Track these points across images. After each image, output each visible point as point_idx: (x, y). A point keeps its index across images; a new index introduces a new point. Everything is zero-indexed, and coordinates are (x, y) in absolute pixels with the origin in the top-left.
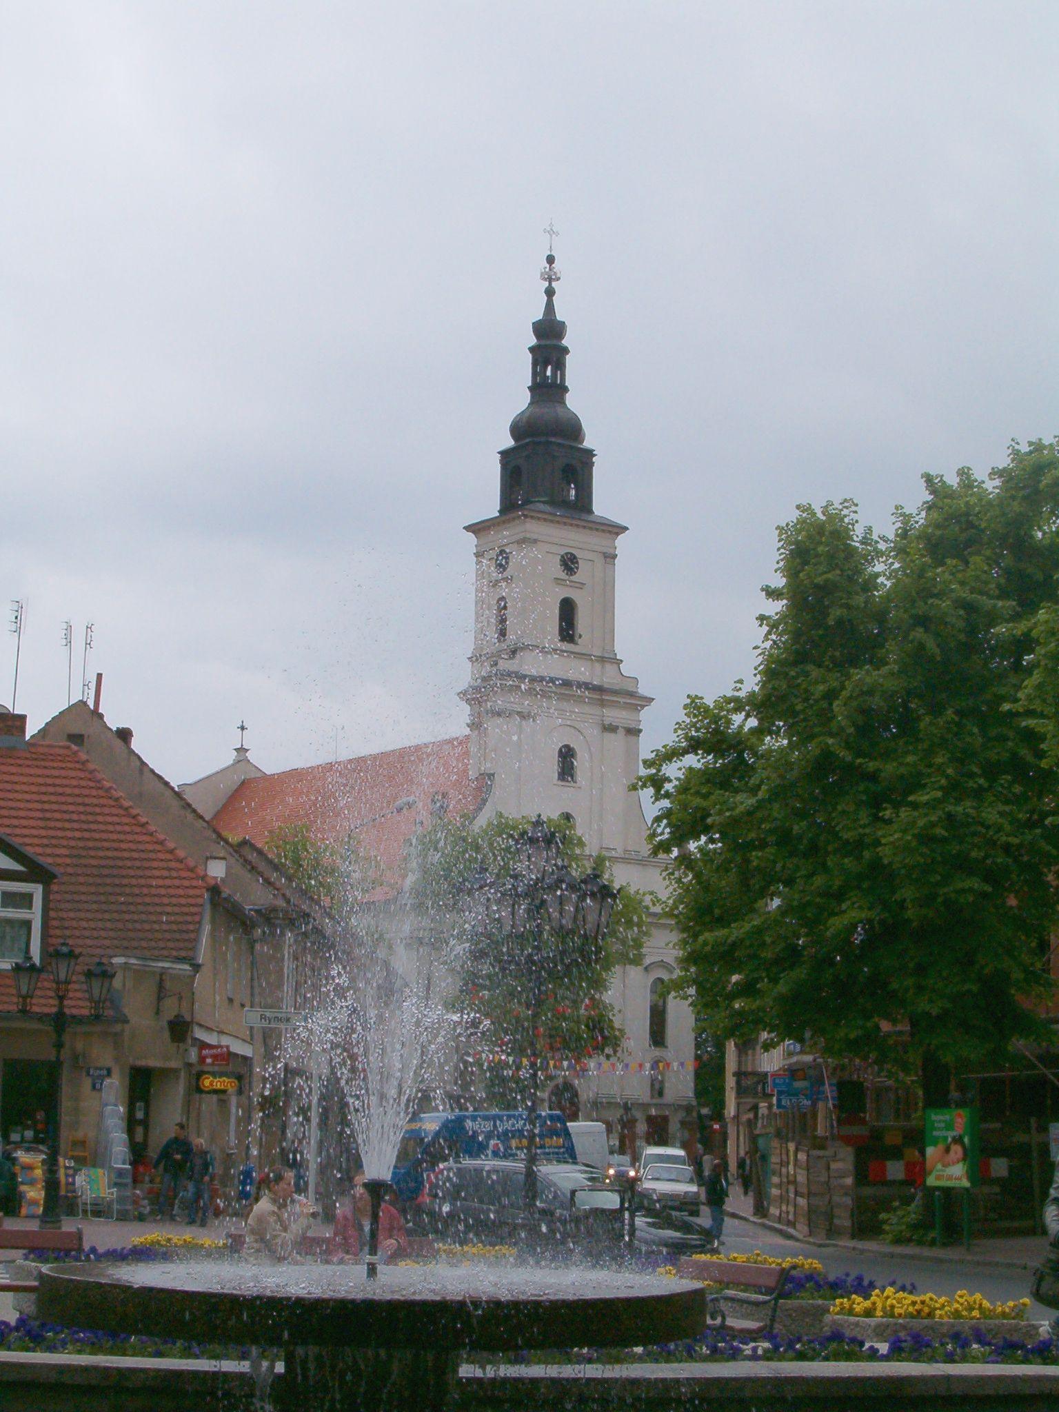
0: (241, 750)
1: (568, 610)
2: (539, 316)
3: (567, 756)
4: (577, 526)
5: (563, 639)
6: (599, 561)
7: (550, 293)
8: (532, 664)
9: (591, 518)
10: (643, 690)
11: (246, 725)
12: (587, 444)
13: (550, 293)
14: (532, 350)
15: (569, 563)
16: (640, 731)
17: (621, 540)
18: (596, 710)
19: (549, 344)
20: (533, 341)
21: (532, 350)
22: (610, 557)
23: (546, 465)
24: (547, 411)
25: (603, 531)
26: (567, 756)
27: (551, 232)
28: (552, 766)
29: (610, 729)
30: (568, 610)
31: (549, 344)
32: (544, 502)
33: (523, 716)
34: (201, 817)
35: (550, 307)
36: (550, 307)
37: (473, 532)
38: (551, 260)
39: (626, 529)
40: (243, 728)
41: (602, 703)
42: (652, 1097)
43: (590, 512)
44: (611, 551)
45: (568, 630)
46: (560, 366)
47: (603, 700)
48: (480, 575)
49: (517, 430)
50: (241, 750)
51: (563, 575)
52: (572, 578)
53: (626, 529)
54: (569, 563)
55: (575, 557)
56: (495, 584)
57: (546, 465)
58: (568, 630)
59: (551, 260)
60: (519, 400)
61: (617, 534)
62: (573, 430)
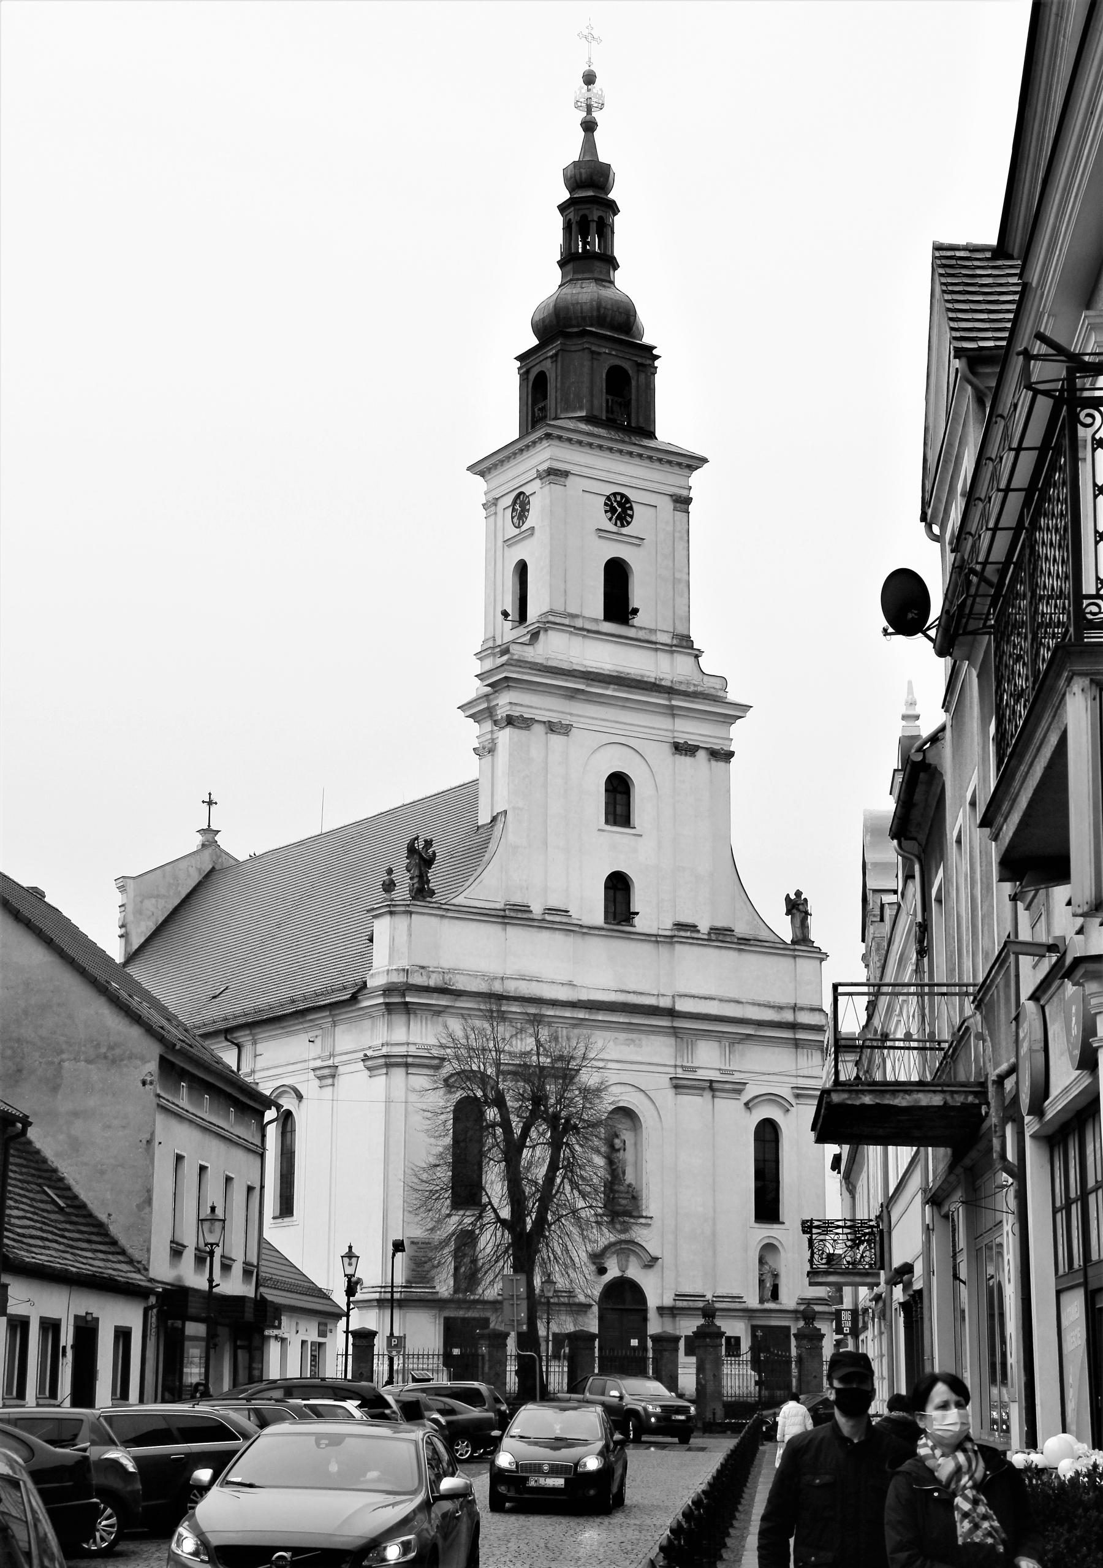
0: (209, 832)
1: (617, 575)
2: (574, 154)
3: (618, 787)
4: (631, 454)
5: (609, 616)
6: (666, 504)
7: (589, 126)
8: (557, 648)
9: (652, 444)
10: (734, 694)
11: (214, 798)
12: (647, 340)
13: (589, 126)
14: (562, 208)
15: (620, 509)
16: (731, 754)
17: (697, 479)
18: (663, 722)
19: (589, 204)
20: (565, 195)
21: (562, 208)
22: (683, 502)
23: (590, 370)
24: (587, 292)
25: (670, 462)
26: (618, 787)
27: (590, 38)
28: (595, 800)
29: (683, 749)
30: (617, 575)
31: (589, 204)
32: (580, 419)
33: (552, 727)
34: (406, 1110)
35: (589, 145)
36: (589, 145)
37: (482, 474)
38: (589, 79)
39: (705, 460)
40: (210, 803)
41: (672, 712)
42: (762, 1301)
43: (652, 435)
44: (684, 493)
45: (618, 604)
46: (605, 230)
47: (672, 707)
48: (492, 534)
50: (209, 832)
51: (610, 526)
52: (624, 530)
53: (705, 460)
54: (620, 509)
55: (628, 500)
56: (509, 542)
57: (590, 370)
58: (618, 604)
59: (589, 79)
60: (542, 281)
61: (692, 468)
62: (619, 324)
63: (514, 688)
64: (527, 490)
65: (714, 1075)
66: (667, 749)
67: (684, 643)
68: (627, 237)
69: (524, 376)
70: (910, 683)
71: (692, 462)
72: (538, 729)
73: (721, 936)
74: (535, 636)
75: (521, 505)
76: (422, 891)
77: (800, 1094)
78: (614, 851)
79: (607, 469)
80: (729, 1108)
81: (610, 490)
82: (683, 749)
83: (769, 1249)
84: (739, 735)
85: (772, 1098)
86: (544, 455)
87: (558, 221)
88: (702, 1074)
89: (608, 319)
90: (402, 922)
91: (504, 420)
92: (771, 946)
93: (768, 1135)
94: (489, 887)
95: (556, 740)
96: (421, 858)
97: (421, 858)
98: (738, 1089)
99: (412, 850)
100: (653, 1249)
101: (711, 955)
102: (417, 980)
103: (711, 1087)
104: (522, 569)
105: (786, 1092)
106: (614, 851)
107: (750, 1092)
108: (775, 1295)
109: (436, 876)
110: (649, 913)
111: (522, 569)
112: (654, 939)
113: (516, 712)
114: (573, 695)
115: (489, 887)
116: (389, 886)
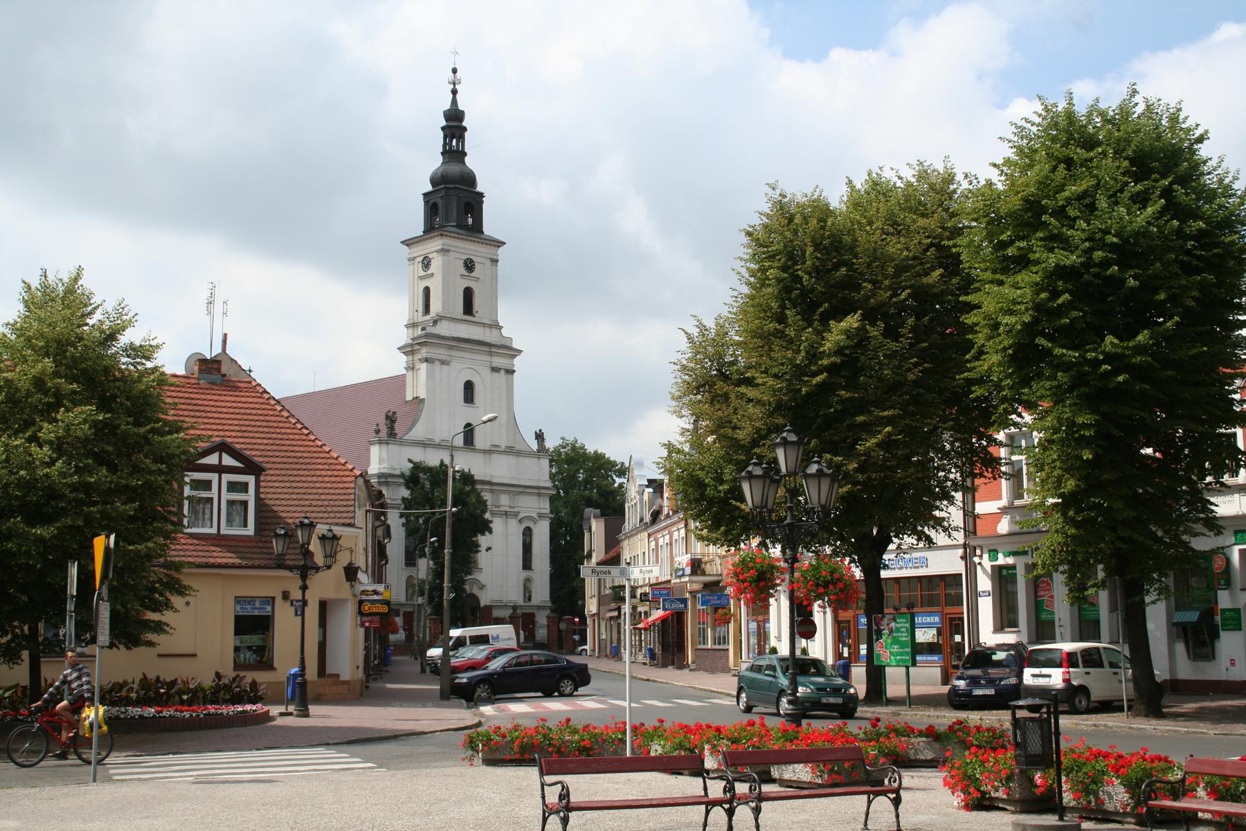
1: (468, 294)
2: (447, 106)
3: (469, 387)
6: (489, 262)
7: (454, 92)
8: (445, 329)
13: (454, 92)
14: (443, 129)
15: (469, 266)
17: (517, 361)
18: (487, 358)
19: (454, 124)
20: (444, 123)
21: (443, 129)
22: (495, 261)
24: (454, 168)
26: (469, 387)
29: (495, 370)
30: (468, 294)
31: (454, 124)
33: (443, 363)
35: (454, 101)
36: (454, 101)
38: (455, 71)
41: (491, 354)
43: (482, 232)
45: (468, 308)
46: (461, 138)
49: (434, 181)
51: (466, 273)
54: (469, 266)
56: (421, 278)
58: (468, 308)
59: (455, 71)
60: (434, 161)
62: (470, 180)
63: (425, 343)
64: (430, 256)
65: (507, 509)
66: (488, 370)
67: (496, 326)
68: (471, 142)
69: (426, 202)
70: (225, 335)
71: (500, 244)
72: (437, 363)
73: (510, 451)
74: (435, 322)
75: (426, 263)
76: (392, 434)
77: (541, 516)
78: (467, 415)
79: (465, 248)
80: (513, 523)
81: (465, 257)
82: (495, 370)
83: (528, 580)
84: (518, 363)
85: (530, 518)
86: (436, 244)
87: (441, 134)
88: (503, 509)
89: (754, 266)
90: (384, 447)
91: (416, 222)
92: (527, 454)
93: (528, 533)
94: (418, 432)
95: (445, 367)
96: (391, 419)
97: (391, 419)
98: (516, 515)
99: (387, 417)
100: (483, 582)
101: (504, 458)
102: (393, 472)
103: (506, 514)
104: (427, 291)
105: (535, 515)
106: (467, 415)
107: (521, 515)
108: (530, 599)
109: (398, 427)
110: (480, 441)
111: (427, 291)
112: (485, 452)
113: (429, 356)
114: (451, 348)
115: (418, 432)
116: (377, 432)
